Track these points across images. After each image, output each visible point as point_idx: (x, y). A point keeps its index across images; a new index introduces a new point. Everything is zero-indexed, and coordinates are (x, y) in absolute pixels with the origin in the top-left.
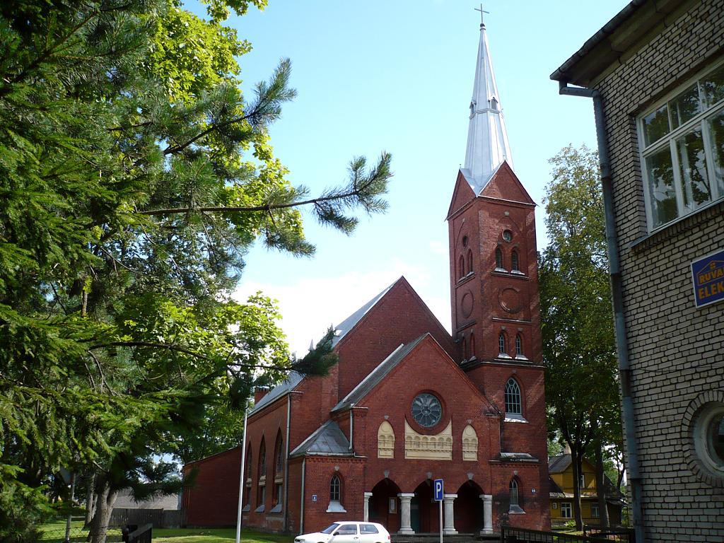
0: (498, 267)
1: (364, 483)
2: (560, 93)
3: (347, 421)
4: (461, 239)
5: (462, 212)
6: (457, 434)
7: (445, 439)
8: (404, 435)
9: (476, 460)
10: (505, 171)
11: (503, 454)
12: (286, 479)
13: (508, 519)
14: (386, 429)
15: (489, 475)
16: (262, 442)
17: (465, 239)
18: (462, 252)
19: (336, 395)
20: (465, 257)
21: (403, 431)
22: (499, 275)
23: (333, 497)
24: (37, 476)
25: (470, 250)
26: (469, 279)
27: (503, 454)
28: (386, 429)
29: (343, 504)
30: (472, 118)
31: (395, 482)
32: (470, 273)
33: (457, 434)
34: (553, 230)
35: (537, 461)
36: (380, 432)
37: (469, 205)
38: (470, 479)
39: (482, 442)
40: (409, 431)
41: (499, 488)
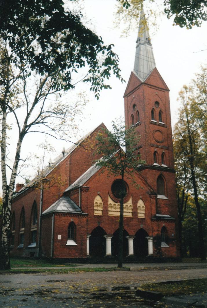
0: (152, 119)
1: (87, 229)
2: (103, 124)
3: (76, 196)
4: (132, 106)
5: (132, 92)
6: (135, 203)
7: (129, 206)
8: (108, 203)
9: (144, 217)
10: (155, 72)
11: (157, 215)
12: (39, 228)
13: (161, 250)
14: (98, 200)
15: (151, 226)
16: (22, 211)
17: (134, 106)
18: (132, 112)
19: (68, 182)
20: (134, 115)
21: (107, 201)
22: (153, 123)
23: (70, 237)
24: (36, 11)
25: (138, 111)
26: (138, 125)
27: (157, 215)
28: (98, 200)
29: (75, 241)
30: (137, 47)
31: (103, 228)
32: (137, 123)
33: (135, 203)
34: (37, 250)
35: (174, 219)
36: (95, 201)
37: (137, 88)
38: (141, 227)
39: (147, 209)
40: (110, 201)
41: (156, 233)
